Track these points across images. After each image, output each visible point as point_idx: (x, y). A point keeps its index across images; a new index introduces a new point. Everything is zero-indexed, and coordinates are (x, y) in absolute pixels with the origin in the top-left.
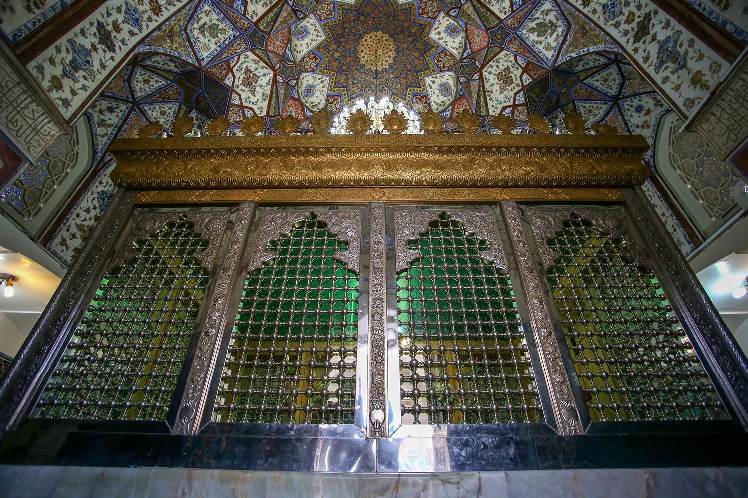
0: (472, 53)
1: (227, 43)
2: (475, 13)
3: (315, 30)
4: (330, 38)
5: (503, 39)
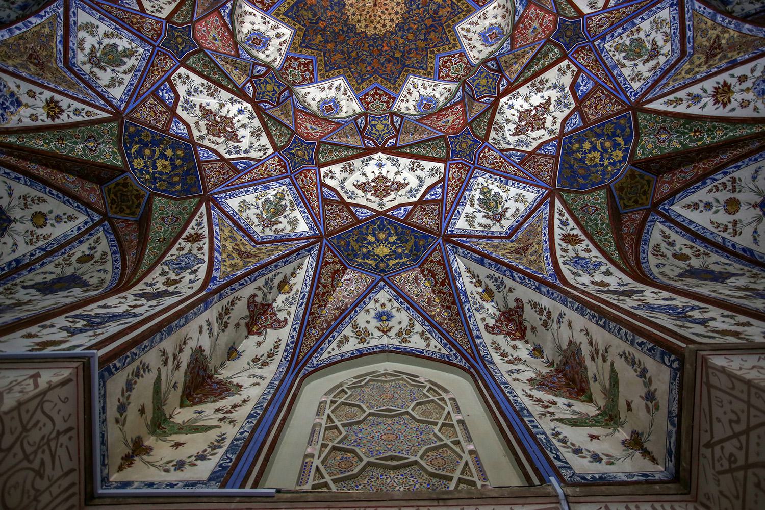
0: (217, 10)
1: (620, 30)
2: (227, 72)
3: (470, 39)
4: (449, 26)
5: (171, 37)
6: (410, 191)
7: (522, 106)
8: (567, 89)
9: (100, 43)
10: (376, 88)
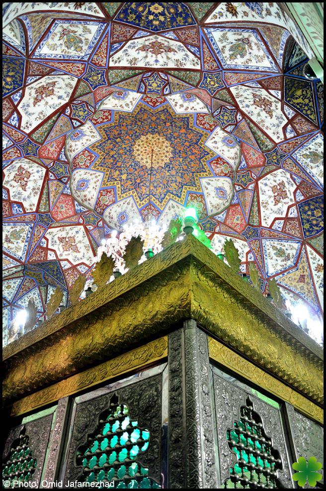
1: (29, 236)
3: (91, 175)
4: (107, 171)
6: (28, 106)
7: (34, 176)
8: (22, 201)
9: (250, 53)
10: (110, 120)
